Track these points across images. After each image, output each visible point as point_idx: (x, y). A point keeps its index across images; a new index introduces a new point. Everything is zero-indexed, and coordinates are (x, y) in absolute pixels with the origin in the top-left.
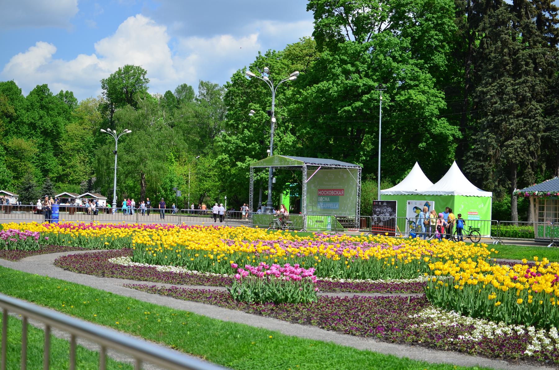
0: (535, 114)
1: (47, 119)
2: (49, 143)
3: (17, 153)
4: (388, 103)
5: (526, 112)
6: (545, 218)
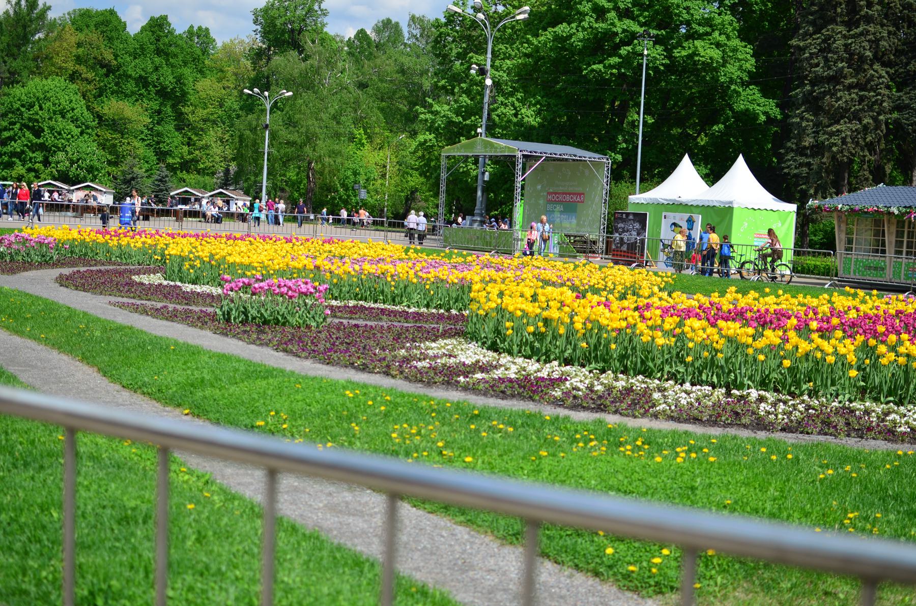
0: (877, 85)
1: (166, 70)
2: (168, 110)
3: (117, 125)
4: (662, 61)
5: (863, 81)
6: (854, 246)
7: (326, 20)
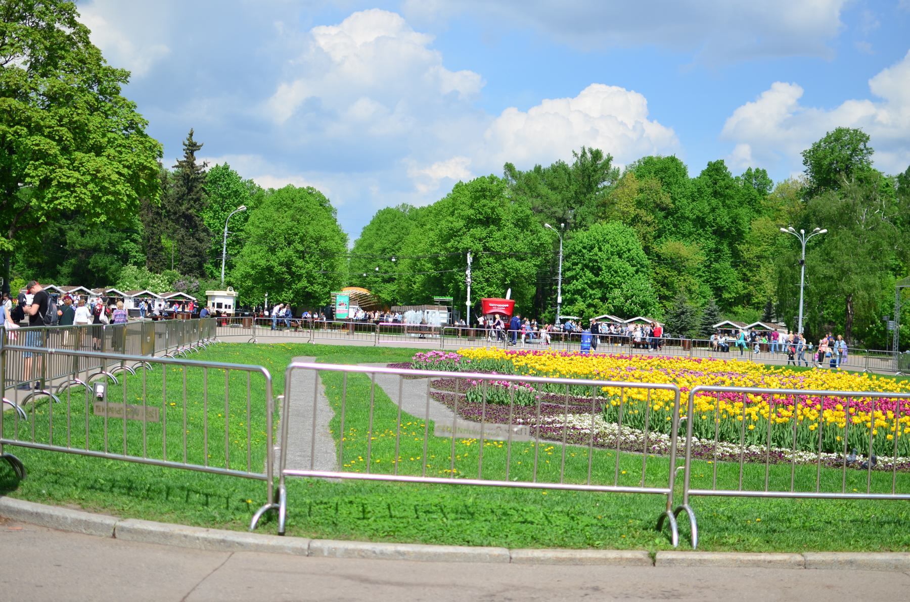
1: (722, 211)
2: (725, 248)
3: (676, 264)
7: (871, 158)
